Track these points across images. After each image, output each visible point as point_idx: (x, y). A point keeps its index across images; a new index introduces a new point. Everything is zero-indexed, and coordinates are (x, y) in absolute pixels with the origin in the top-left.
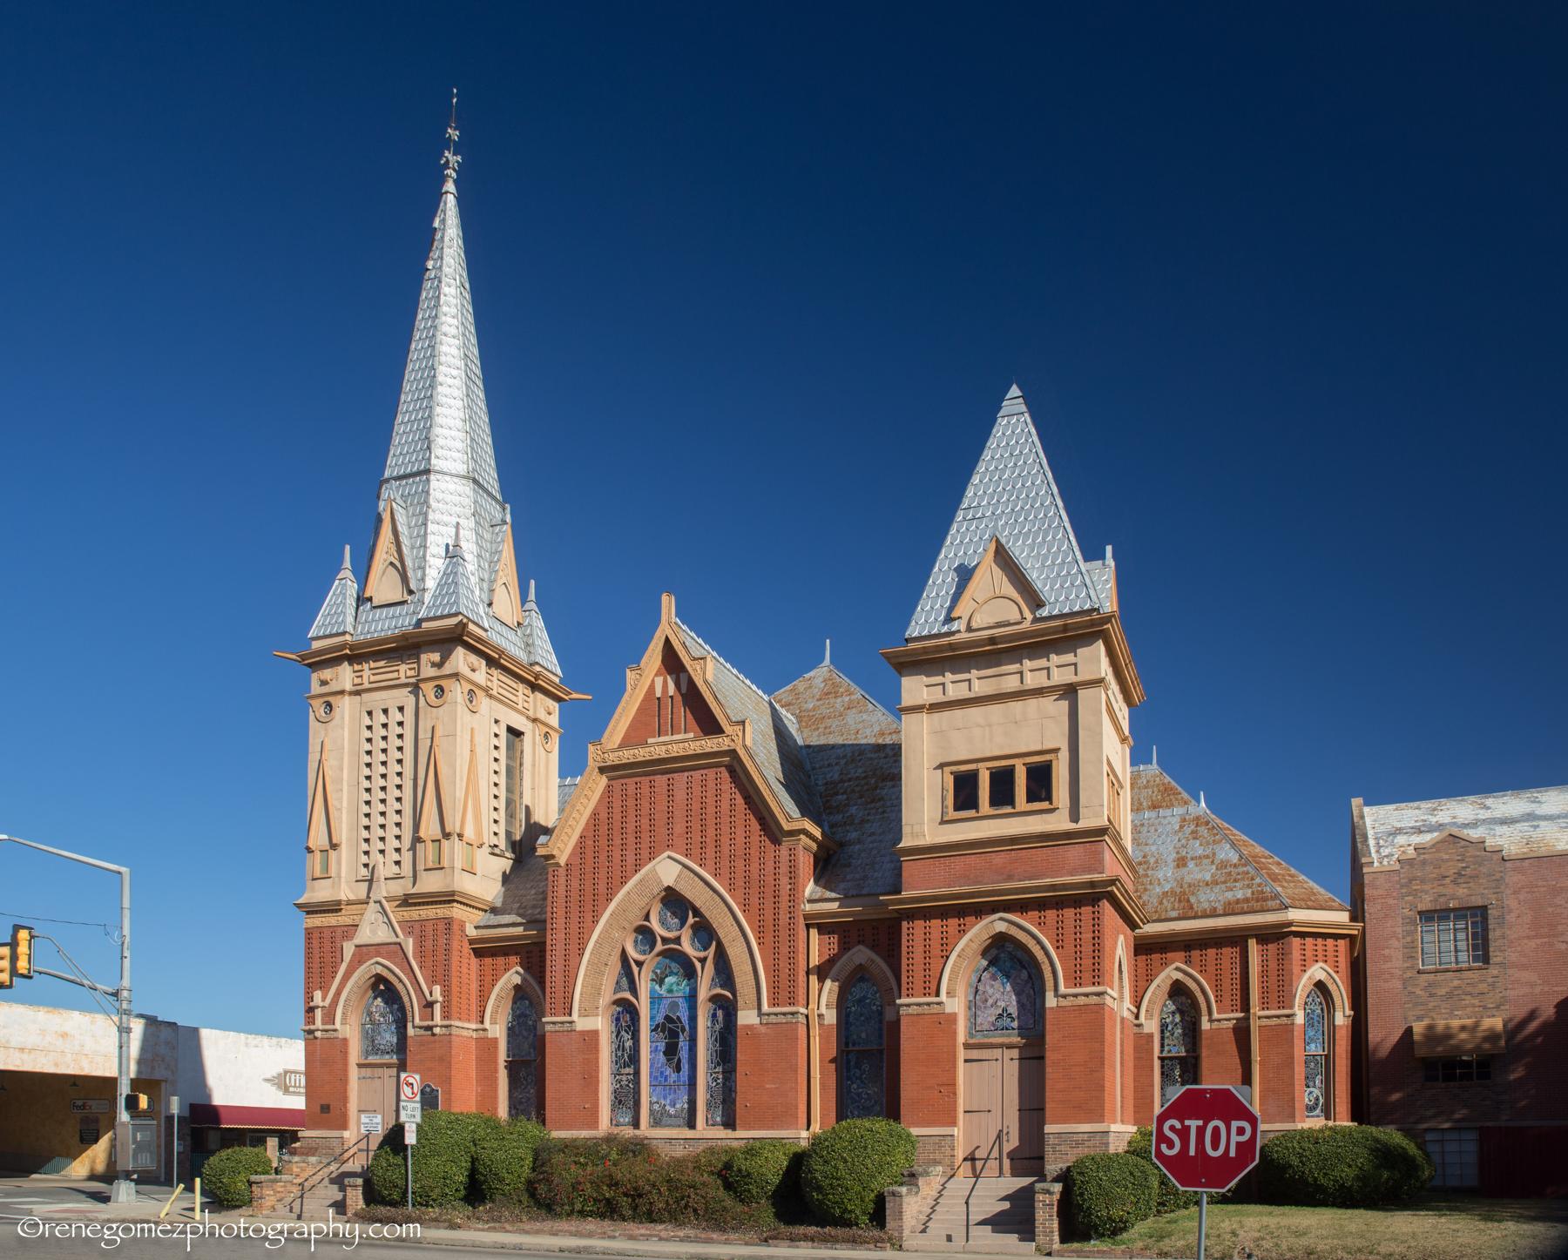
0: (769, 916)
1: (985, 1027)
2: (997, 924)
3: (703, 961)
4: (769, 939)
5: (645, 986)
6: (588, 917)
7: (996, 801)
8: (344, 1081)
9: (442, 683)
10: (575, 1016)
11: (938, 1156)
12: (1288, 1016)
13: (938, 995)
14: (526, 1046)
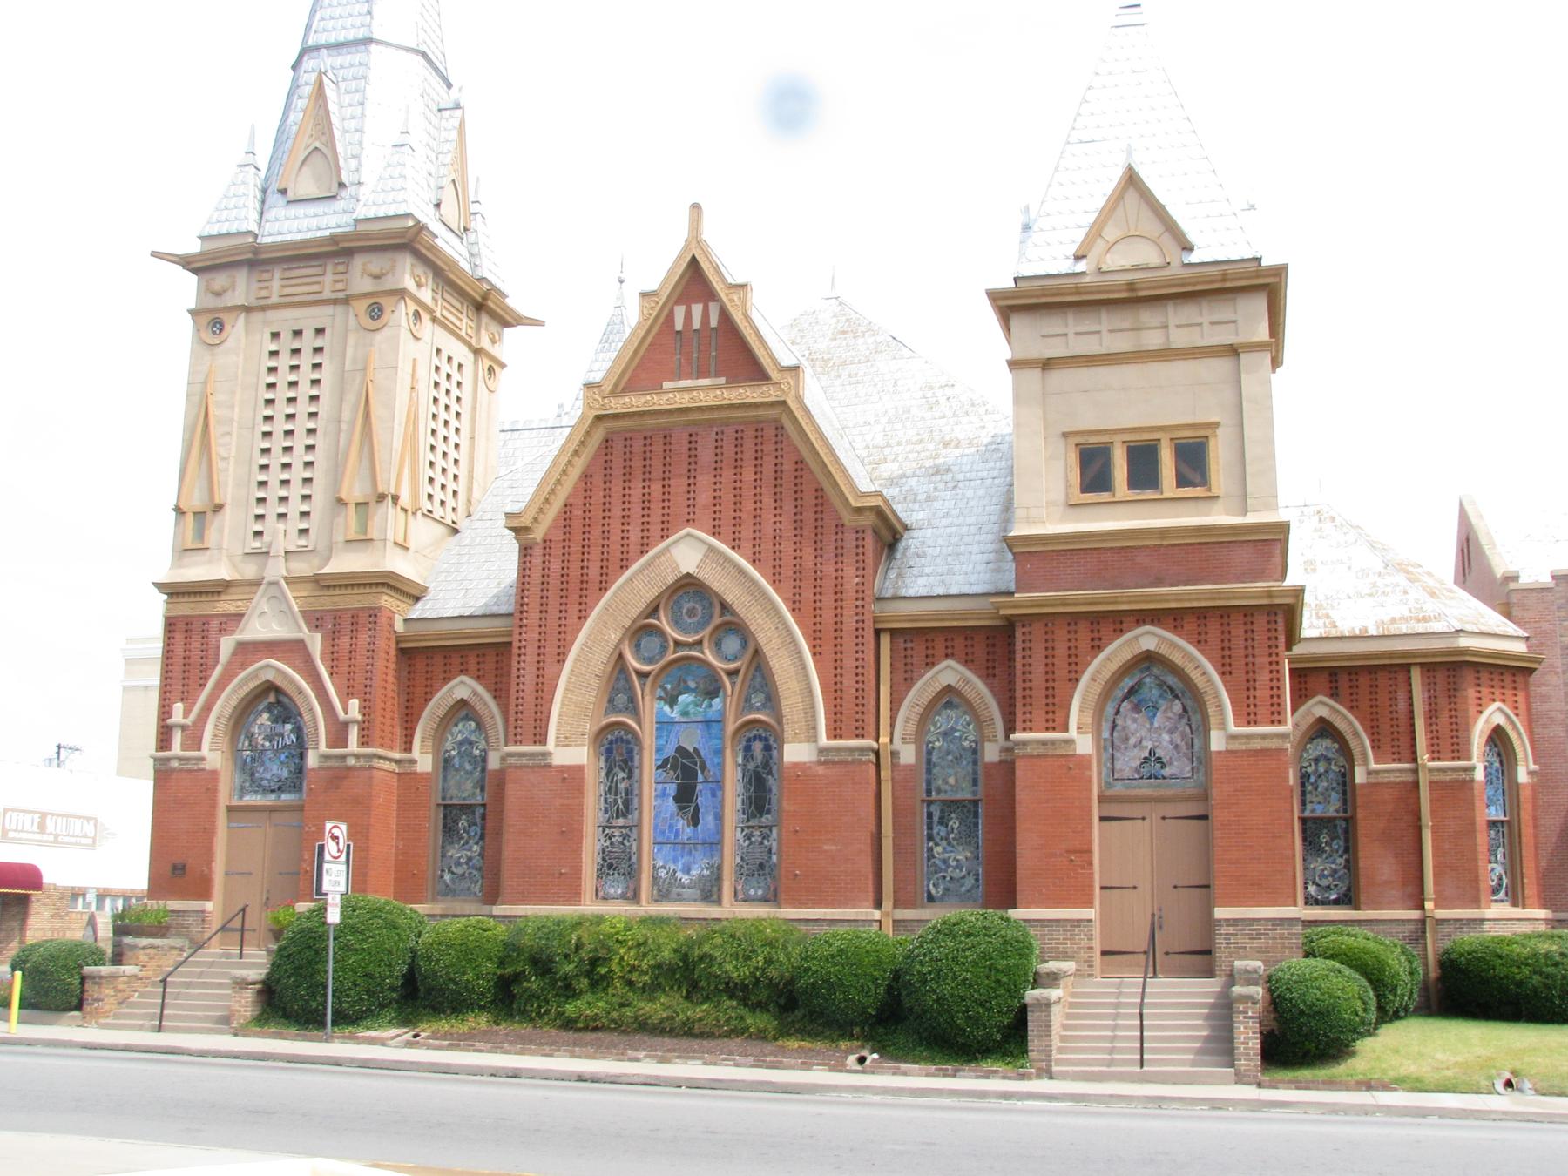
0: (828, 616)
1: (1127, 774)
2: (1148, 639)
3: (732, 674)
4: (828, 649)
5: (652, 707)
6: (573, 611)
7: (1135, 482)
8: (210, 832)
12: (1466, 770)
13: (1066, 729)
14: (469, 785)
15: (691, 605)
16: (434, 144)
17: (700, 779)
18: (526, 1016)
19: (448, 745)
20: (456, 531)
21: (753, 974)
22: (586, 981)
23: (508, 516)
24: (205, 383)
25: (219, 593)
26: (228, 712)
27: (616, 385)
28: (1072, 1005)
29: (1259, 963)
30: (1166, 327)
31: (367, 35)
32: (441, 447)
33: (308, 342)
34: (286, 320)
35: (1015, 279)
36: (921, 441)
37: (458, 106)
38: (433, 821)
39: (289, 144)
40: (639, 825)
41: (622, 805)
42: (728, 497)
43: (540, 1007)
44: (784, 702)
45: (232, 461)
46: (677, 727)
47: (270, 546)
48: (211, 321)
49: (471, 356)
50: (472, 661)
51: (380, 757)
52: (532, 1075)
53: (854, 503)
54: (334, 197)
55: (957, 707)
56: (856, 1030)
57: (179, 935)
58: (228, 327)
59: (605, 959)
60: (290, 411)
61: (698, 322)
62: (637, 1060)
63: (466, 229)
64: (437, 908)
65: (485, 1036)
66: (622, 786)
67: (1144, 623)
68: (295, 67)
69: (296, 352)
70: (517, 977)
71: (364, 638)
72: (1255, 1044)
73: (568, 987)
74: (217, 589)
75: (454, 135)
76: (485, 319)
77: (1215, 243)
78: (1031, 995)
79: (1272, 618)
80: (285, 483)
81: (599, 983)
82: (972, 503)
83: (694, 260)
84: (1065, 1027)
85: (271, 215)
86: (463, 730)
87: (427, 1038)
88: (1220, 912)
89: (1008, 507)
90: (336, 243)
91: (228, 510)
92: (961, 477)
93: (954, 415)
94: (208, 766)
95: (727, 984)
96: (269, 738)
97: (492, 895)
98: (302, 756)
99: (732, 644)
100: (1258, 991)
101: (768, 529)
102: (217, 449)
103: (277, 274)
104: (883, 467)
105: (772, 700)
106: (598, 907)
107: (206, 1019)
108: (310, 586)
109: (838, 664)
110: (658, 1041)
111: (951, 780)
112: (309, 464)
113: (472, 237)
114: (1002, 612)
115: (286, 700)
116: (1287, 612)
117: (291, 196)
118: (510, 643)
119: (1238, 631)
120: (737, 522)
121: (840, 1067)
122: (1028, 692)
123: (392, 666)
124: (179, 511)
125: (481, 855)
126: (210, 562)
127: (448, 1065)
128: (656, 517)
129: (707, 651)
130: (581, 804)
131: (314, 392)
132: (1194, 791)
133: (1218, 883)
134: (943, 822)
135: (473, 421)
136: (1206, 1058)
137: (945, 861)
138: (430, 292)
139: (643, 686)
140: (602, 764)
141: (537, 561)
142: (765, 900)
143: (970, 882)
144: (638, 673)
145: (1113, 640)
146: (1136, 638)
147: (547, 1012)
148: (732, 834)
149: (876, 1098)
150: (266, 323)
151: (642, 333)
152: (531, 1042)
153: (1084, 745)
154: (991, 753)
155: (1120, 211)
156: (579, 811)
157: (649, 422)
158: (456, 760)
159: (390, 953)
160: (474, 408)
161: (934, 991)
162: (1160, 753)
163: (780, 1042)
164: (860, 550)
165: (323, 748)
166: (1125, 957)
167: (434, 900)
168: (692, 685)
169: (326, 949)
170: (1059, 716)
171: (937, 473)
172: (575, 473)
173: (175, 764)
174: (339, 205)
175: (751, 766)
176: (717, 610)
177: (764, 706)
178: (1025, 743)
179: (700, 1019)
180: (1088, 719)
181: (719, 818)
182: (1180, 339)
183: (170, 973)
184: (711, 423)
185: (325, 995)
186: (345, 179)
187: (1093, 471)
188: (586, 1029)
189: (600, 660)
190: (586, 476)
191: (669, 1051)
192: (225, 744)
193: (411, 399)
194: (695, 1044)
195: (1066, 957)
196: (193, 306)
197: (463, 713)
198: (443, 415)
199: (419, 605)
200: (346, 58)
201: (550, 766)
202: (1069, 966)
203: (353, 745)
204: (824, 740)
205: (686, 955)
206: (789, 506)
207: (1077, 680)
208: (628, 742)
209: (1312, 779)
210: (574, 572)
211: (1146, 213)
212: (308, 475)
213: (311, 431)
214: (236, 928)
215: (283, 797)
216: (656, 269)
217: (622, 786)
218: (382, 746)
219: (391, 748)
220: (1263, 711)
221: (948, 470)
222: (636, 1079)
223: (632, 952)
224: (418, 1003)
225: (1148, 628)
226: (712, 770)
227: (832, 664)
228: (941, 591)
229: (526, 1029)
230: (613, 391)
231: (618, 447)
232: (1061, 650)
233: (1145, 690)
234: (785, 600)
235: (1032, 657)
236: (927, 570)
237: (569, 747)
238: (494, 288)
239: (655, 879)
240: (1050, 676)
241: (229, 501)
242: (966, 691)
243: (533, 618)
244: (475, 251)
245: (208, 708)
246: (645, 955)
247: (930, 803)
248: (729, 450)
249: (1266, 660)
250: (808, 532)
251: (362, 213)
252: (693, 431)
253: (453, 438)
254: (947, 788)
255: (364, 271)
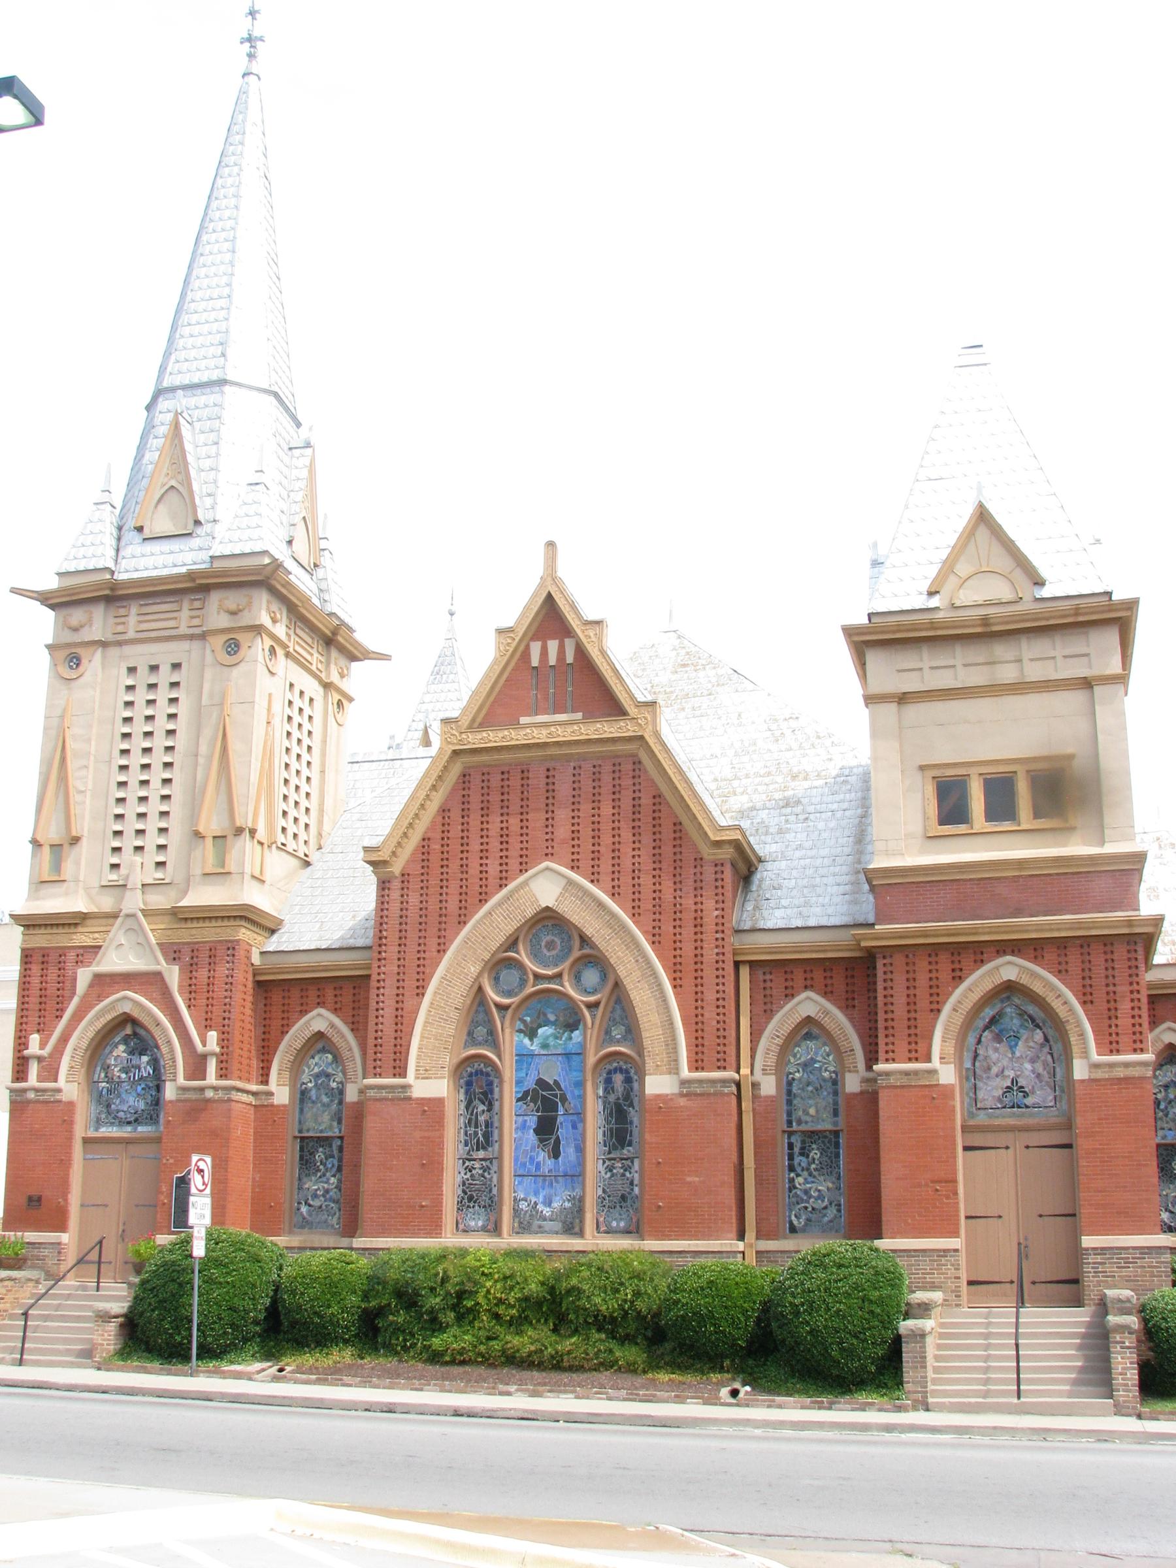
0: (688, 948)
1: (988, 1104)
2: (1009, 969)
3: (592, 1006)
4: (688, 982)
5: (511, 1040)
8: (65, 1163)
9: (239, 636)
10: (411, 1078)
11: (937, 1278)
13: (928, 1059)
14: (326, 1117)
15: (549, 938)
16: (285, 482)
17: (561, 1111)
18: (391, 1350)
19: (305, 1078)
20: (307, 864)
21: (621, 1307)
22: (452, 1315)
23: (367, 849)
24: (62, 717)
25: (76, 924)
26: (85, 1043)
27: (473, 720)
28: (942, 1336)
29: (1127, 1293)
30: (1019, 661)
31: (222, 376)
32: (294, 781)
33: (165, 676)
34: (141, 655)
35: (870, 615)
36: (769, 774)
37: (308, 445)
38: (290, 1153)
39: (145, 482)
40: (500, 1158)
41: (482, 1137)
42: (586, 832)
43: (405, 1340)
44: (644, 1034)
45: (89, 794)
46: (537, 1060)
47: (127, 877)
48: (68, 656)
49: (321, 690)
50: (330, 993)
51: (239, 1090)
52: (407, 1409)
53: (713, 837)
54: (190, 534)
55: (816, 1038)
56: (727, 1363)
57: (33, 1267)
58: (84, 661)
59: (471, 1292)
60: (147, 744)
61: (555, 657)
62: (509, 1394)
63: (316, 565)
64: (295, 1241)
65: (350, 1370)
66: (482, 1119)
67: (1005, 953)
68: (148, 408)
69: (152, 687)
70: (381, 1312)
71: (222, 970)
72: (1133, 1375)
73: (434, 1320)
74: (74, 921)
75: (304, 473)
76: (334, 653)
77: (1066, 578)
78: (906, 1326)
79: (1132, 947)
80: (142, 816)
81: (465, 1316)
82: (825, 835)
83: (549, 597)
84: (937, 1358)
85: (126, 552)
86: (320, 1062)
87: (292, 1372)
88: (1088, 1241)
89: (861, 837)
90: (193, 580)
91: (84, 842)
92: (811, 809)
93: (801, 747)
94: (64, 1097)
95: (596, 1317)
96: (125, 1070)
97: (351, 1228)
98: (159, 1088)
99: (591, 977)
100: (1133, 1321)
101: (627, 863)
102: (74, 782)
103: (134, 610)
104: (732, 800)
105: (632, 1033)
106: (459, 1240)
107: (68, 1352)
108: (167, 918)
109: (698, 996)
110: (526, 1374)
111: (812, 1111)
112: (166, 798)
113: (320, 573)
114: (863, 944)
115: (142, 1032)
116: (1143, 939)
117: (147, 533)
118: (369, 976)
119: (1098, 960)
120: (596, 856)
121: (713, 1401)
122: (890, 1023)
123: (250, 998)
124: (36, 843)
125: (338, 1188)
126: (67, 894)
127: (322, 1400)
128: (514, 852)
129: (567, 984)
130: (442, 1137)
131: (171, 727)
132: (1057, 1120)
133: (1085, 1212)
134: (804, 1153)
135: (323, 754)
136: (1084, 1389)
137: (806, 1192)
138: (284, 628)
139: (503, 1018)
140: (462, 1097)
141: (395, 895)
142: (627, 1232)
143: (831, 1212)
144: (497, 1005)
145: (974, 971)
146: (997, 968)
147: (414, 1345)
148: (594, 1166)
149: (758, 1432)
150: (122, 657)
151: (498, 669)
152: (398, 1376)
153: (947, 1075)
154: (852, 1084)
155: (971, 547)
156: (440, 1145)
157: (505, 756)
158: (313, 1092)
159: (254, 1286)
160: (324, 742)
161: (808, 1323)
162: (1022, 1082)
163: (650, 1375)
164: (719, 883)
165: (181, 1080)
166: (991, 1286)
167: (290, 1232)
168: (552, 1018)
169: (190, 1282)
170: (921, 1047)
171: (787, 805)
172: (433, 807)
173: (31, 1095)
174: (195, 542)
175: (612, 1098)
176: (577, 942)
177: (624, 1038)
178: (887, 1074)
179: (569, 1352)
180: (950, 1049)
181: (581, 1150)
182: (1035, 672)
183: (32, 1306)
184: (568, 758)
185: (190, 1329)
186: (201, 518)
187: (951, 805)
188: (453, 1362)
189: (460, 993)
190: (444, 810)
191: (539, 1384)
192: (81, 1075)
193: (267, 733)
194: (565, 1377)
195: (933, 1287)
196: (50, 642)
197: (320, 1045)
198: (296, 749)
199: (275, 937)
200: (201, 399)
201: (410, 1098)
202: (937, 1296)
203: (211, 1078)
204: (685, 1073)
205: (553, 1288)
206: (647, 839)
207: (939, 1011)
208: (488, 1075)
209: (1162, 1106)
210: (433, 905)
211: (997, 549)
212: (165, 808)
213: (168, 765)
214: (93, 1260)
215: (140, 1129)
216: (513, 605)
217: (482, 1119)
218: (240, 1078)
219: (248, 1080)
220: (1125, 1039)
221: (798, 802)
222: (513, 1414)
223: (499, 1286)
224: (280, 1337)
225: (1009, 958)
226: (573, 1102)
227: (693, 997)
228: (799, 923)
229: (391, 1363)
230: (470, 727)
231: (476, 780)
232: (922, 980)
233: (1006, 1020)
234: (645, 933)
235: (893, 987)
236: (784, 902)
237: (430, 1081)
238: (343, 623)
239: (516, 1212)
240: (912, 1007)
241: (86, 834)
242: (826, 1022)
243: (392, 951)
244: (323, 586)
245: (64, 1039)
246: (512, 1288)
247: (790, 1134)
248: (587, 784)
249: (1127, 988)
250: (667, 865)
251: (218, 550)
252: (550, 765)
253: (305, 772)
254: (808, 1119)
255: (220, 607)
